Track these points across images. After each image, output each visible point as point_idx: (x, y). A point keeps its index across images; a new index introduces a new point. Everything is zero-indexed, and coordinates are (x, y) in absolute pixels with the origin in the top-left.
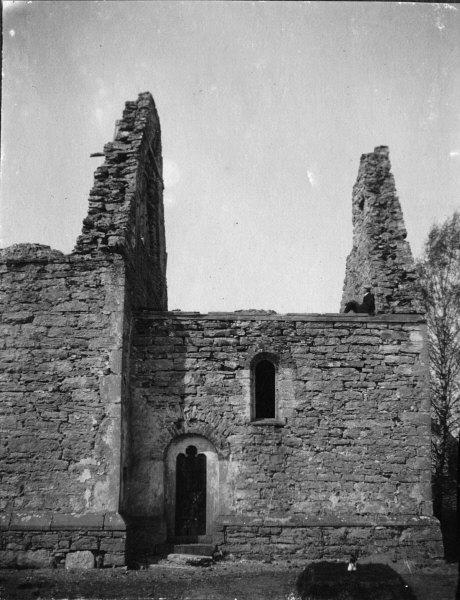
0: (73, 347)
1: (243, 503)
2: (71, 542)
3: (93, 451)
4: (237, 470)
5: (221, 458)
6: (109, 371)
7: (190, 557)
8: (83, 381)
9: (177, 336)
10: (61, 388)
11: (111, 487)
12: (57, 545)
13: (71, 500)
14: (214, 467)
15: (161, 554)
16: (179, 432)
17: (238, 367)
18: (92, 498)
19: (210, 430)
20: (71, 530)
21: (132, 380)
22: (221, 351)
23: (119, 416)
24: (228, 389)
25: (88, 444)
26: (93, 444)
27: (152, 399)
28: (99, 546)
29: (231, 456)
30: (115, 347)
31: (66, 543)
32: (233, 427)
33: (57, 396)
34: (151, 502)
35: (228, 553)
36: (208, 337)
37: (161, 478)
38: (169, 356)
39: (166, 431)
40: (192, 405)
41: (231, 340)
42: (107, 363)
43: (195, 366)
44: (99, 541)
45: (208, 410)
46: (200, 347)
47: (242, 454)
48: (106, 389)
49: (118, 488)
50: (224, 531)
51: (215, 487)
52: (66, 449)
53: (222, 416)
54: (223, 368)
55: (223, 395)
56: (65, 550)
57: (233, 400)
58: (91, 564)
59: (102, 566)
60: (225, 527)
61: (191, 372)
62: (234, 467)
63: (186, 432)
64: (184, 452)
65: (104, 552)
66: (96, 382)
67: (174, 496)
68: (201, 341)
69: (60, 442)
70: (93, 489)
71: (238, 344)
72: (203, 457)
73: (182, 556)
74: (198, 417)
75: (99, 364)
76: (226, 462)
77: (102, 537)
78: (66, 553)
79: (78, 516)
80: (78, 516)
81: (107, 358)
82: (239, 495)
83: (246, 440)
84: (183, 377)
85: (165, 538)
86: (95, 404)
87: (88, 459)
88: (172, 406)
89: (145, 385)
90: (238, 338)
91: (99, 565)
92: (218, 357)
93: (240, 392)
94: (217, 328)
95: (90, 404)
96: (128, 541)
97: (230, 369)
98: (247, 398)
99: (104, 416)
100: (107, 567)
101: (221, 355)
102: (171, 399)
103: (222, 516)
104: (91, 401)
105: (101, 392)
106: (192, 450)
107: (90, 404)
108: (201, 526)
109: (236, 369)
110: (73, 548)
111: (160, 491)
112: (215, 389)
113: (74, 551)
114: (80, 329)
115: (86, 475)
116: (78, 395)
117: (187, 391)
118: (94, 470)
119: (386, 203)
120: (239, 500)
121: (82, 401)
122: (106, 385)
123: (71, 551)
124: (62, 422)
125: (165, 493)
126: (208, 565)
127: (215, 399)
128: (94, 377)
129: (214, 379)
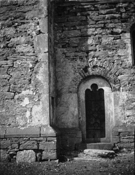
0: (16, 18)
1: (131, 118)
2: (19, 145)
3: (31, 86)
4: (126, 97)
5: (114, 90)
6: (40, 32)
7: (100, 152)
8: (23, 39)
9: (82, 15)
10: (9, 45)
11: (44, 109)
12: (10, 147)
13: (17, 118)
14: (109, 96)
15: (80, 148)
16: (86, 74)
17: (122, 32)
18: (31, 117)
19: (106, 73)
20: (19, 137)
21: (56, 44)
22: (111, 23)
23: (47, 61)
24: (116, 46)
25: (27, 81)
26: (30, 80)
27: (68, 55)
28: (38, 147)
29: (121, 88)
30: (43, 16)
31: (16, 145)
32: (122, 70)
33: (6, 51)
34: (71, 120)
35: (123, 148)
36: (102, 14)
37: (76, 104)
38: (78, 28)
39: (78, 74)
40: (94, 57)
41: (117, 15)
42: (38, 27)
43: (94, 33)
44: (38, 144)
45: (104, 60)
46: (97, 21)
47: (129, 87)
48: (38, 43)
49: (48, 109)
50: (119, 135)
51: (111, 109)
52: (12, 85)
53: (114, 63)
54: (112, 33)
55: (114, 50)
56: (16, 150)
57: (120, 52)
58: (33, 159)
59: (41, 160)
60: (120, 133)
61: (92, 37)
62: (124, 95)
63: (91, 74)
64: (89, 88)
65: (41, 151)
66: (31, 40)
67: (84, 116)
68: (97, 17)
69: (9, 80)
70: (31, 111)
71: (121, 18)
72: (102, 91)
73: (94, 151)
74: (98, 64)
75: (33, 28)
76: (118, 92)
77: (40, 141)
78: (16, 152)
79: (23, 128)
80: (23, 128)
81: (38, 24)
82: (128, 113)
83: (130, 78)
84: (87, 40)
85: (81, 140)
86: (31, 54)
87: (27, 91)
88: (81, 59)
89: (63, 47)
90: (121, 14)
91: (40, 160)
92: (108, 27)
93: (124, 46)
94: (107, 9)
95: (28, 54)
96: (58, 143)
97: (117, 33)
98: (130, 51)
99: (37, 62)
100: (45, 160)
101: (111, 25)
102: (80, 54)
103: (117, 126)
104: (29, 52)
105: (35, 46)
106: (94, 86)
107: (28, 54)
108: (102, 132)
109: (121, 33)
110: (21, 148)
111: (76, 113)
112: (108, 46)
113: (22, 150)
114: (19, 6)
115: (26, 101)
116: (19, 49)
117: (90, 48)
118: (31, 98)
119: (131, 68)
120: (128, 116)
121: (22, 52)
122: (38, 40)
123: (20, 150)
124: (9, 67)
125: (79, 113)
126: (113, 157)
127: (109, 52)
128: (30, 37)
129: (107, 40)
